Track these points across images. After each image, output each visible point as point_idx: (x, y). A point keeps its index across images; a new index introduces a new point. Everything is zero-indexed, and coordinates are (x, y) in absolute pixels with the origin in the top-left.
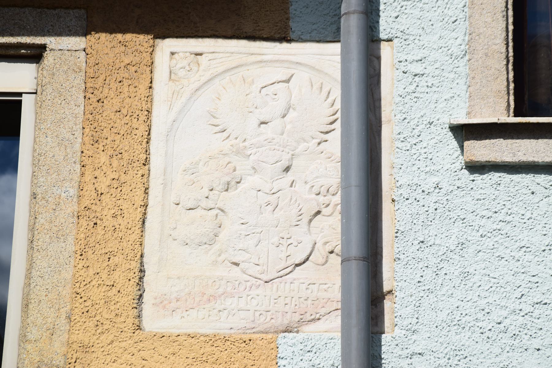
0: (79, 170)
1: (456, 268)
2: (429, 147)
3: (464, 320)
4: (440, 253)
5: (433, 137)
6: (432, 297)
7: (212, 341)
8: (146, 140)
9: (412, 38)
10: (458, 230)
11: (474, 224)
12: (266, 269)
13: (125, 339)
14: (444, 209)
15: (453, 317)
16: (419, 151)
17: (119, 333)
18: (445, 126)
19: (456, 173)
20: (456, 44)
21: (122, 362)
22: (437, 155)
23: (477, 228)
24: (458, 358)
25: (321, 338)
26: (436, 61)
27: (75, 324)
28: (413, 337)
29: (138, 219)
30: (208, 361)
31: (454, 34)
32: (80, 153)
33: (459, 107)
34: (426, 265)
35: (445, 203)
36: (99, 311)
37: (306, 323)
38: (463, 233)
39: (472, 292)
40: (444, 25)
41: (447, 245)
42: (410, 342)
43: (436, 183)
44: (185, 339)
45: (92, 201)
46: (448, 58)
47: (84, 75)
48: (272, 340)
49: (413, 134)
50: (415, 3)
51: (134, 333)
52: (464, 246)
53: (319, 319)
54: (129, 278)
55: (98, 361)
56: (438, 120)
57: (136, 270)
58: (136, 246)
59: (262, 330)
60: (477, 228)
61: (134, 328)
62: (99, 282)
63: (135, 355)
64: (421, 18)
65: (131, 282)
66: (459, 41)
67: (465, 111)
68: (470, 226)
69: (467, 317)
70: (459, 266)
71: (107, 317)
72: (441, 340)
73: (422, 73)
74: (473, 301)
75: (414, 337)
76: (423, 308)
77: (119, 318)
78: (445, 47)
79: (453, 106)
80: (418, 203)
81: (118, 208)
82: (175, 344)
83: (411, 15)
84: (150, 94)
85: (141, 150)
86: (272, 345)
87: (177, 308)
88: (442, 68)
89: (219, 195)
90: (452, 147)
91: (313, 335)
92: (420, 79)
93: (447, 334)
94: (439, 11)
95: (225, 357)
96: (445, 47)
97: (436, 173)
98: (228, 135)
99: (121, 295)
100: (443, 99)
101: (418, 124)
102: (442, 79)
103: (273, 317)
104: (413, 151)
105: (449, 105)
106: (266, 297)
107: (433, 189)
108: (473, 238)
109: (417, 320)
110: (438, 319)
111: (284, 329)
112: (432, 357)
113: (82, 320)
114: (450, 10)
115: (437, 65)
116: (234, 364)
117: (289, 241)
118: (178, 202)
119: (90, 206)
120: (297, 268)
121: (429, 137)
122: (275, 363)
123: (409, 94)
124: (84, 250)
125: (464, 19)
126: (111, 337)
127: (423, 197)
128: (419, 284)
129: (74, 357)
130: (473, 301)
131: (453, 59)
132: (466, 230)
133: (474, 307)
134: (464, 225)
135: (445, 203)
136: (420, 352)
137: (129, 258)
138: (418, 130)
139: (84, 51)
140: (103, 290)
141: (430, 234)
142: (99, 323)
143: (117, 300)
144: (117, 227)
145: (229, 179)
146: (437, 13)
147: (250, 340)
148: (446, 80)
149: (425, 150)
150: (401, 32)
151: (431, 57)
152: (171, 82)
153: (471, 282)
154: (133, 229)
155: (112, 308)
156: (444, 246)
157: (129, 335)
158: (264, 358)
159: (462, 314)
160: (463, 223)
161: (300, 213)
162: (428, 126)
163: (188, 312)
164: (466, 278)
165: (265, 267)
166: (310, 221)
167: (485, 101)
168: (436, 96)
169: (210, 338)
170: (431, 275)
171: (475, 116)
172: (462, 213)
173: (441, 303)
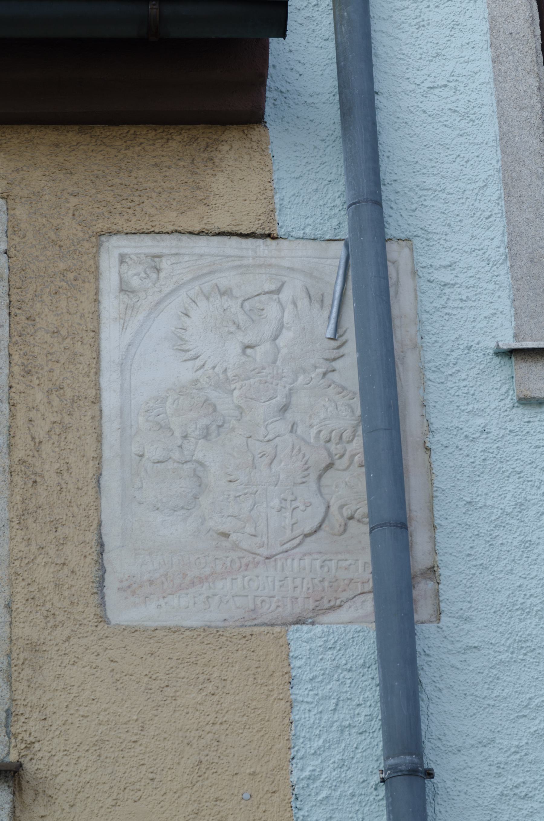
0: (7, 411)
1: (515, 536)
2: (470, 379)
3: (529, 602)
4: (493, 518)
5: (473, 365)
6: (486, 574)
7: (201, 637)
8: (95, 370)
9: (436, 237)
10: (514, 487)
11: (533, 478)
12: (266, 541)
13: (85, 635)
14: (495, 460)
15: (515, 599)
16: (457, 384)
17: (77, 626)
18: (488, 351)
19: (506, 413)
20: (494, 246)
21: (84, 664)
22: (480, 389)
23: (537, 484)
24: (523, 651)
25: (345, 630)
26: (469, 268)
27: (18, 614)
28: (464, 626)
29: (90, 475)
30: (199, 662)
31: (488, 233)
32: (8, 388)
33: (504, 327)
34: (476, 533)
35: (496, 452)
36: (48, 598)
37: (324, 611)
38: (520, 491)
39: (536, 566)
40: (475, 221)
41: (502, 506)
42: (462, 633)
43: (482, 425)
44: (165, 634)
45: (28, 452)
46: (484, 264)
47: (7, 284)
48: (281, 635)
49: (447, 362)
50: (436, 193)
51: (96, 626)
52: (523, 507)
53: (340, 606)
54: (84, 554)
55: (52, 663)
56: (478, 343)
57: (93, 544)
58: (90, 512)
59: (266, 622)
60: (537, 484)
61: (96, 620)
62: (45, 560)
63: (101, 655)
64: (446, 212)
65: (88, 560)
66: (496, 242)
67: (511, 332)
68: (528, 481)
69: (532, 599)
70: (518, 533)
71: (59, 605)
72: (501, 629)
73: (452, 282)
74: (538, 578)
75: (467, 627)
76: (476, 589)
77: (75, 607)
78: (479, 250)
79: (495, 326)
80: (461, 452)
81: (62, 461)
82: (152, 641)
83: (432, 208)
84: (96, 309)
85: (88, 384)
86: (282, 641)
87: (151, 594)
88: (478, 276)
89: (196, 444)
90: (499, 379)
91: (335, 627)
92: (452, 290)
93: (508, 621)
94: (467, 203)
95: (221, 657)
96: (479, 250)
97: (481, 413)
98: (202, 364)
99: (76, 577)
100: (482, 317)
101: (453, 348)
102: (479, 290)
103: (280, 603)
104: (450, 384)
105: (490, 324)
106: (269, 579)
107: (478, 434)
108: (534, 497)
109: (469, 605)
110: (496, 603)
111: (295, 620)
112: (491, 652)
113: (27, 609)
114: (482, 203)
115: (471, 273)
116: (233, 666)
117: (294, 505)
118: (141, 453)
119: (26, 458)
120: (308, 539)
121: (468, 366)
122: (287, 664)
123: (437, 309)
124: (23, 517)
125: (500, 215)
126: (67, 632)
127: (467, 444)
128: (468, 558)
129: (22, 656)
130: (538, 578)
131: (490, 265)
132: (524, 487)
133: (540, 586)
134: (521, 480)
135: (496, 452)
136: (476, 645)
137: (83, 527)
138: (453, 357)
139: (6, 253)
140: (51, 570)
141: (480, 493)
142: (49, 613)
143: (70, 583)
144: (64, 486)
145: (209, 422)
146: (465, 207)
147: (252, 635)
148: (485, 292)
149: (465, 383)
150: (422, 229)
151: (462, 262)
152: (123, 293)
153: (535, 554)
154: (85, 488)
155: (66, 593)
156: (497, 508)
157: (90, 628)
158: (271, 657)
159: (525, 595)
160: (519, 478)
161: (307, 466)
162: (466, 351)
163: (166, 600)
164: (529, 549)
165: (265, 539)
166: (320, 477)
167: (536, 320)
168: (473, 312)
169: (198, 633)
170: (483, 546)
171: (524, 340)
172: (518, 465)
173: (498, 582)
